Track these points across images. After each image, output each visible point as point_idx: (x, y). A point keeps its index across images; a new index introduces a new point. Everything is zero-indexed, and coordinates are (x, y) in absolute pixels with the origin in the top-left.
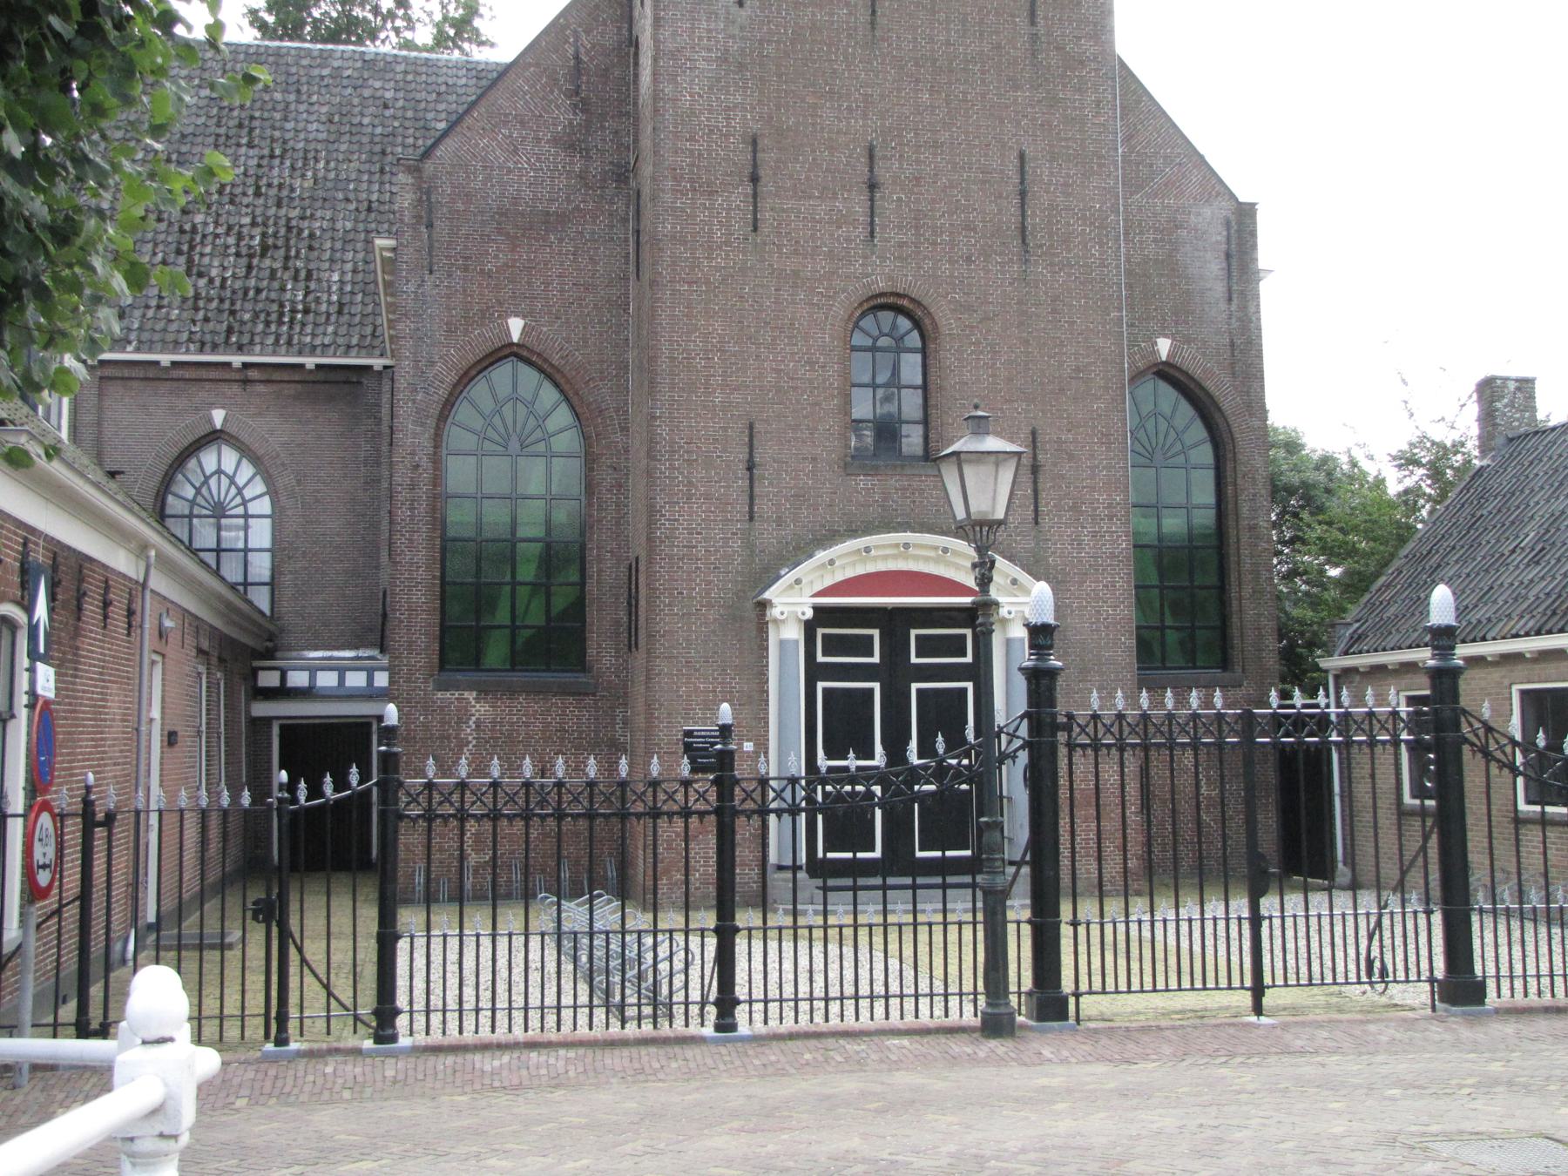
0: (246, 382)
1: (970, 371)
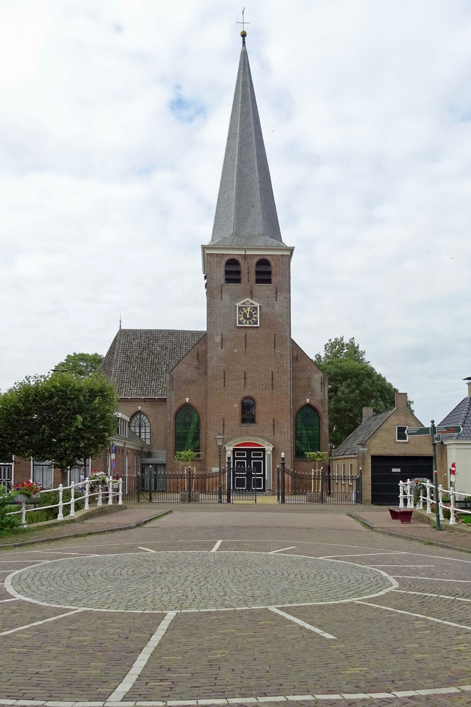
0: (145, 401)
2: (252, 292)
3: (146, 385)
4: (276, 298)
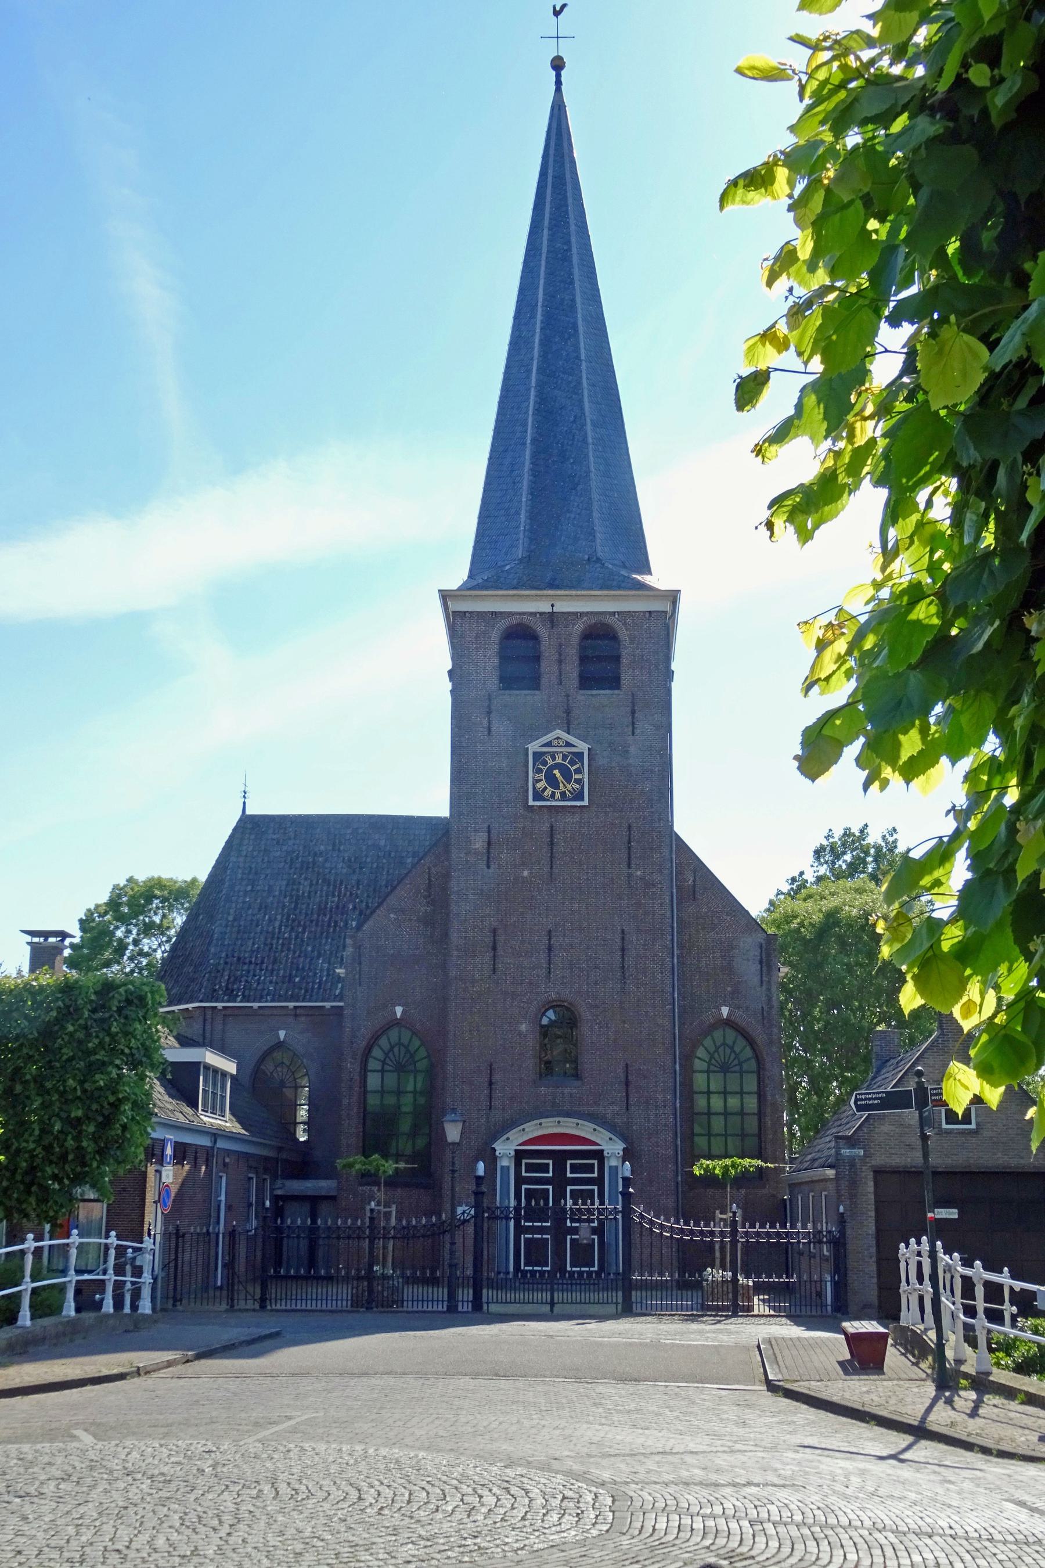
0: (296, 1015)
2: (568, 712)
3: (303, 968)
4: (633, 728)
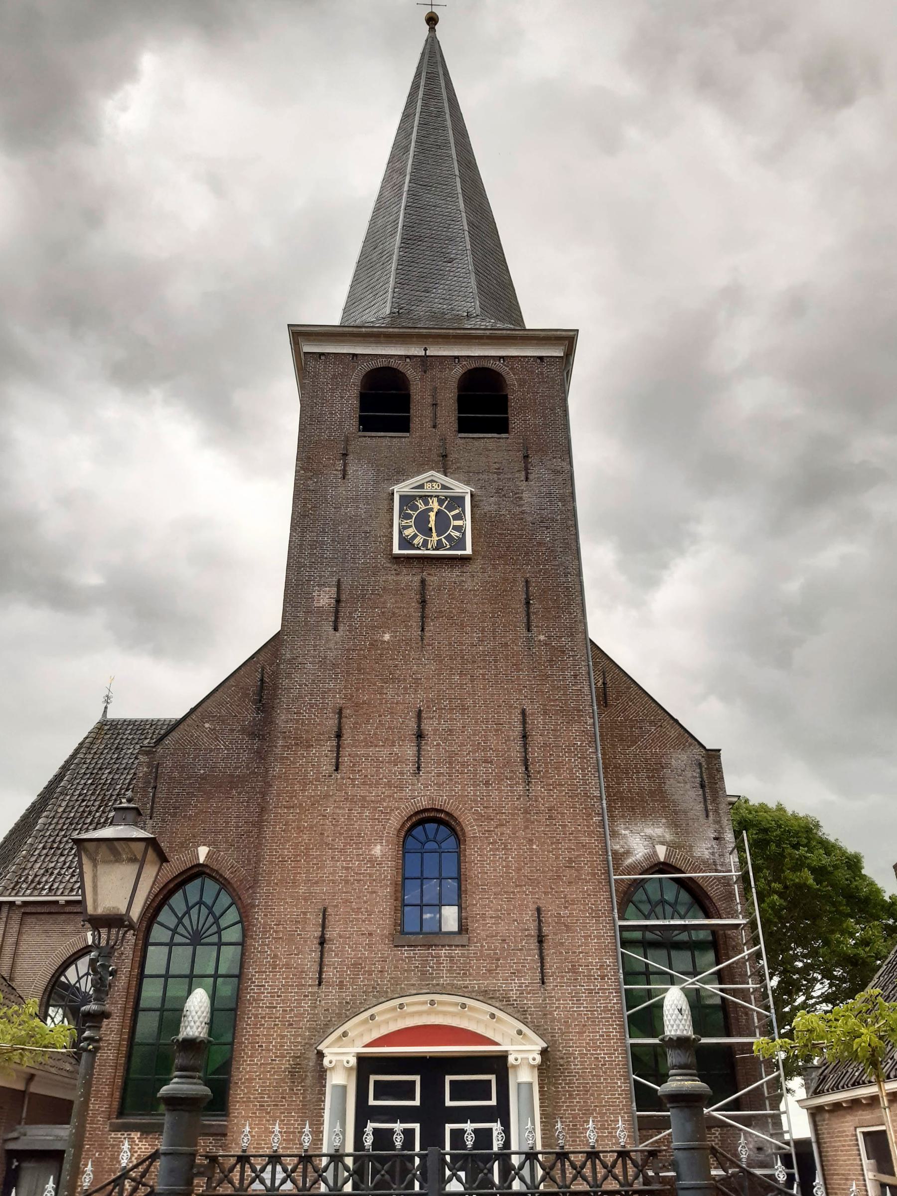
1: (489, 864)
